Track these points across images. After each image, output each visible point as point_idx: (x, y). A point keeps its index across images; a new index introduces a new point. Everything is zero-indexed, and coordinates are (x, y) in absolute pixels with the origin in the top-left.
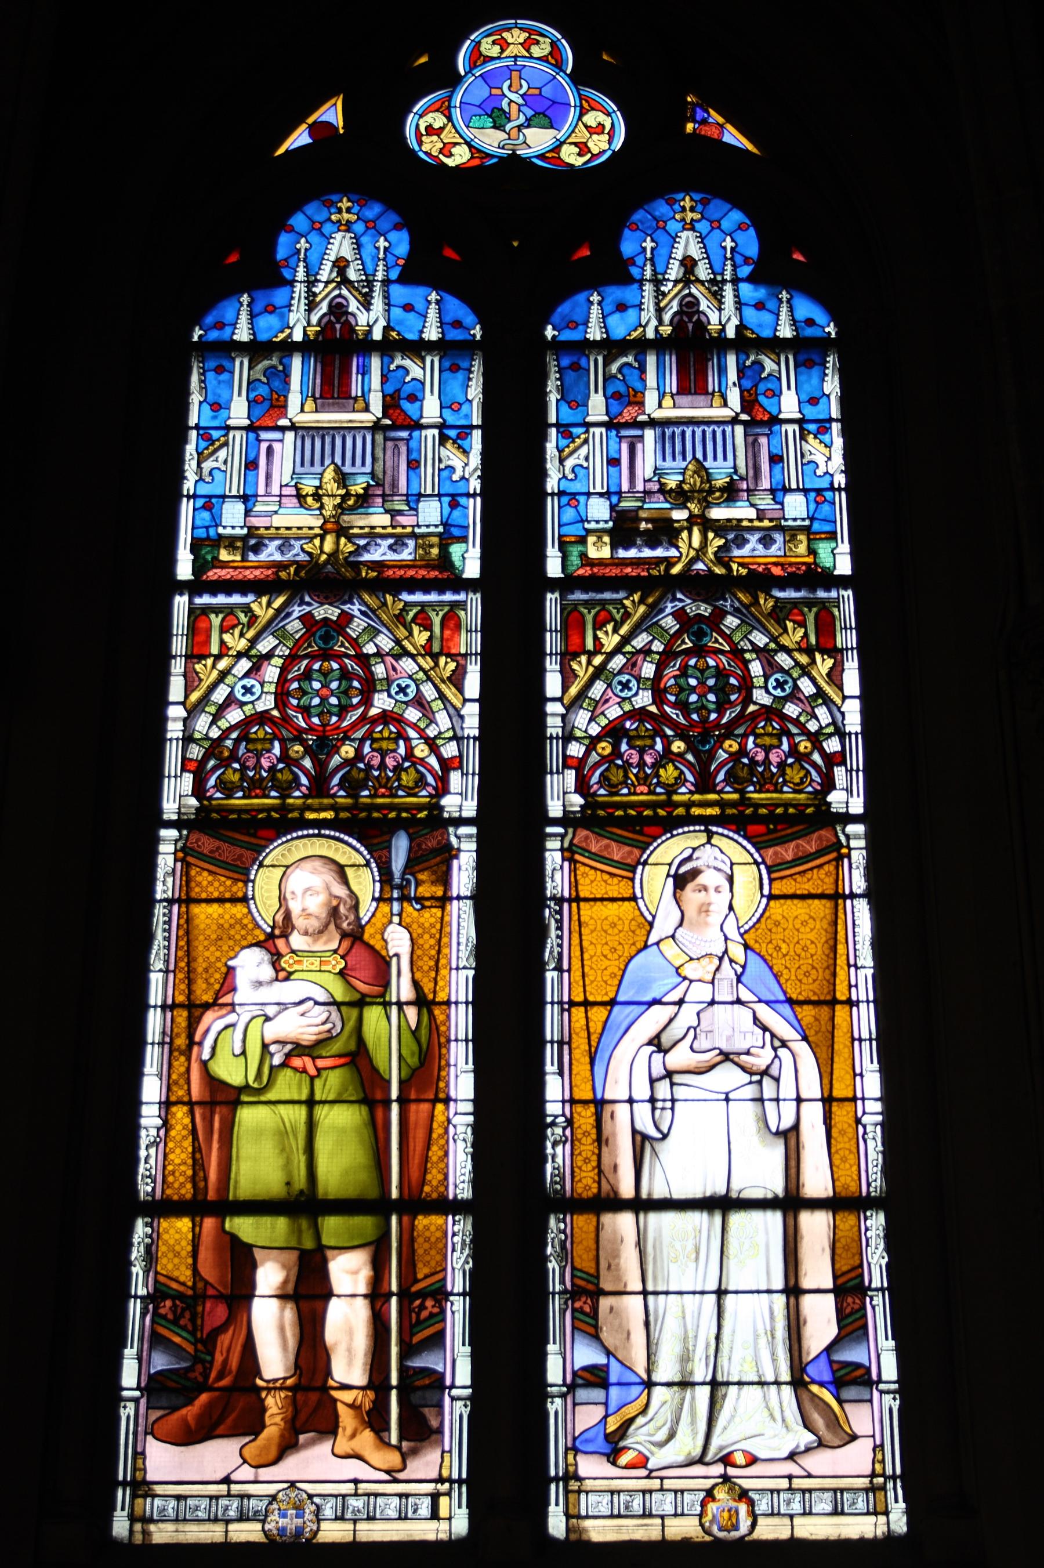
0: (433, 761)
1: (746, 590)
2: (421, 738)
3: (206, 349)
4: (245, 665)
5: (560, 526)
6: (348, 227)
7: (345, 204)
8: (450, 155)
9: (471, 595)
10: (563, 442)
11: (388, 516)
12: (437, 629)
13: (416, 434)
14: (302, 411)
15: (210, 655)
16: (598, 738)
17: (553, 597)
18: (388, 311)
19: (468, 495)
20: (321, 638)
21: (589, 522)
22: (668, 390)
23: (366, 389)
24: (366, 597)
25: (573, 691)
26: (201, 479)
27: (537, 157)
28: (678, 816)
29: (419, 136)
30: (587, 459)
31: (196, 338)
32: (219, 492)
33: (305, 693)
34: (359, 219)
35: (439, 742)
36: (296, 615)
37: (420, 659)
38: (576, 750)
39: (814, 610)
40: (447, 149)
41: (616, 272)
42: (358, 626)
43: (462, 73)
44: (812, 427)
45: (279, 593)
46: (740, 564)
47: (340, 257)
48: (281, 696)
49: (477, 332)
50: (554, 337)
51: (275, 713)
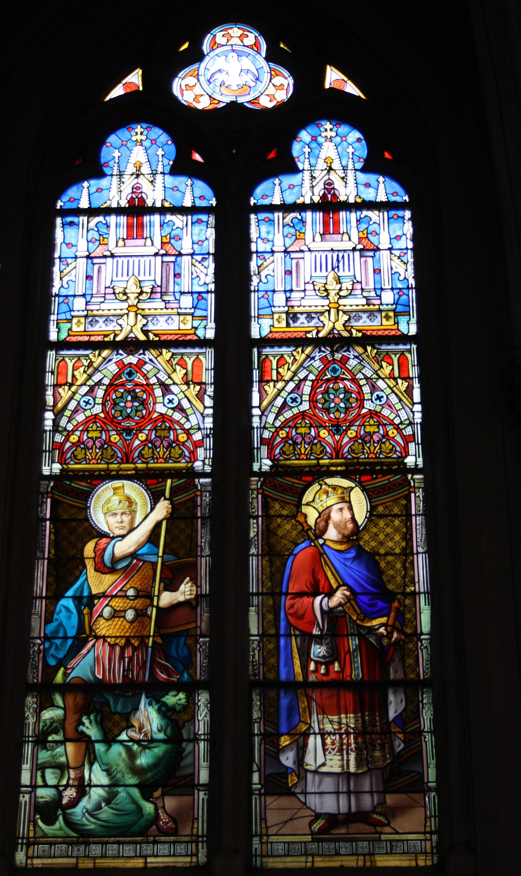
0: (398, 438)
1: (359, 345)
2: (181, 429)
3: (64, 213)
4: (291, 385)
5: (258, 309)
6: (141, 143)
7: (328, 126)
8: (198, 102)
9: (208, 349)
10: (63, 267)
11: (365, 300)
12: (189, 368)
13: (179, 259)
14: (117, 246)
15: (272, 380)
16: (73, 431)
17: (210, 350)
18: (357, 187)
19: (208, 292)
20: (127, 374)
21: (73, 311)
22: (318, 231)
23: (152, 235)
24: (152, 351)
25: (265, 403)
26: (62, 286)
27: (247, 102)
28: (306, 471)
29: (182, 91)
30: (273, 271)
31: (58, 207)
32: (71, 293)
33: (326, 401)
34: (147, 138)
35: (192, 432)
36: (114, 360)
37: (387, 380)
38: (266, 435)
39: (398, 356)
40: (196, 98)
41: (97, 171)
42: (352, 363)
43: (206, 53)
44: (199, 258)
45: (308, 346)
46: (357, 330)
47: (137, 161)
48: (313, 401)
49: (214, 202)
50: (254, 203)
51: (102, 415)
